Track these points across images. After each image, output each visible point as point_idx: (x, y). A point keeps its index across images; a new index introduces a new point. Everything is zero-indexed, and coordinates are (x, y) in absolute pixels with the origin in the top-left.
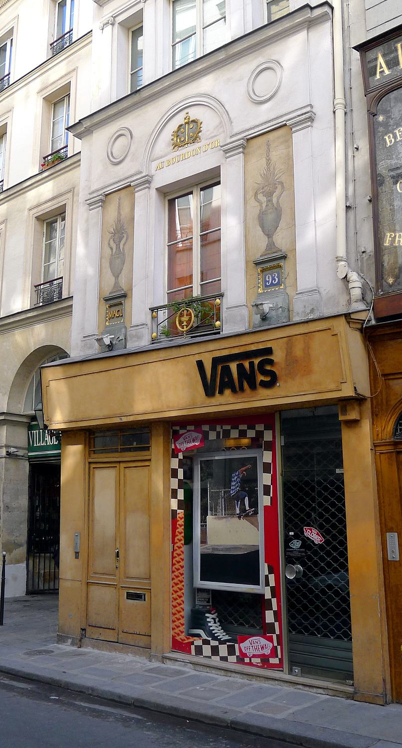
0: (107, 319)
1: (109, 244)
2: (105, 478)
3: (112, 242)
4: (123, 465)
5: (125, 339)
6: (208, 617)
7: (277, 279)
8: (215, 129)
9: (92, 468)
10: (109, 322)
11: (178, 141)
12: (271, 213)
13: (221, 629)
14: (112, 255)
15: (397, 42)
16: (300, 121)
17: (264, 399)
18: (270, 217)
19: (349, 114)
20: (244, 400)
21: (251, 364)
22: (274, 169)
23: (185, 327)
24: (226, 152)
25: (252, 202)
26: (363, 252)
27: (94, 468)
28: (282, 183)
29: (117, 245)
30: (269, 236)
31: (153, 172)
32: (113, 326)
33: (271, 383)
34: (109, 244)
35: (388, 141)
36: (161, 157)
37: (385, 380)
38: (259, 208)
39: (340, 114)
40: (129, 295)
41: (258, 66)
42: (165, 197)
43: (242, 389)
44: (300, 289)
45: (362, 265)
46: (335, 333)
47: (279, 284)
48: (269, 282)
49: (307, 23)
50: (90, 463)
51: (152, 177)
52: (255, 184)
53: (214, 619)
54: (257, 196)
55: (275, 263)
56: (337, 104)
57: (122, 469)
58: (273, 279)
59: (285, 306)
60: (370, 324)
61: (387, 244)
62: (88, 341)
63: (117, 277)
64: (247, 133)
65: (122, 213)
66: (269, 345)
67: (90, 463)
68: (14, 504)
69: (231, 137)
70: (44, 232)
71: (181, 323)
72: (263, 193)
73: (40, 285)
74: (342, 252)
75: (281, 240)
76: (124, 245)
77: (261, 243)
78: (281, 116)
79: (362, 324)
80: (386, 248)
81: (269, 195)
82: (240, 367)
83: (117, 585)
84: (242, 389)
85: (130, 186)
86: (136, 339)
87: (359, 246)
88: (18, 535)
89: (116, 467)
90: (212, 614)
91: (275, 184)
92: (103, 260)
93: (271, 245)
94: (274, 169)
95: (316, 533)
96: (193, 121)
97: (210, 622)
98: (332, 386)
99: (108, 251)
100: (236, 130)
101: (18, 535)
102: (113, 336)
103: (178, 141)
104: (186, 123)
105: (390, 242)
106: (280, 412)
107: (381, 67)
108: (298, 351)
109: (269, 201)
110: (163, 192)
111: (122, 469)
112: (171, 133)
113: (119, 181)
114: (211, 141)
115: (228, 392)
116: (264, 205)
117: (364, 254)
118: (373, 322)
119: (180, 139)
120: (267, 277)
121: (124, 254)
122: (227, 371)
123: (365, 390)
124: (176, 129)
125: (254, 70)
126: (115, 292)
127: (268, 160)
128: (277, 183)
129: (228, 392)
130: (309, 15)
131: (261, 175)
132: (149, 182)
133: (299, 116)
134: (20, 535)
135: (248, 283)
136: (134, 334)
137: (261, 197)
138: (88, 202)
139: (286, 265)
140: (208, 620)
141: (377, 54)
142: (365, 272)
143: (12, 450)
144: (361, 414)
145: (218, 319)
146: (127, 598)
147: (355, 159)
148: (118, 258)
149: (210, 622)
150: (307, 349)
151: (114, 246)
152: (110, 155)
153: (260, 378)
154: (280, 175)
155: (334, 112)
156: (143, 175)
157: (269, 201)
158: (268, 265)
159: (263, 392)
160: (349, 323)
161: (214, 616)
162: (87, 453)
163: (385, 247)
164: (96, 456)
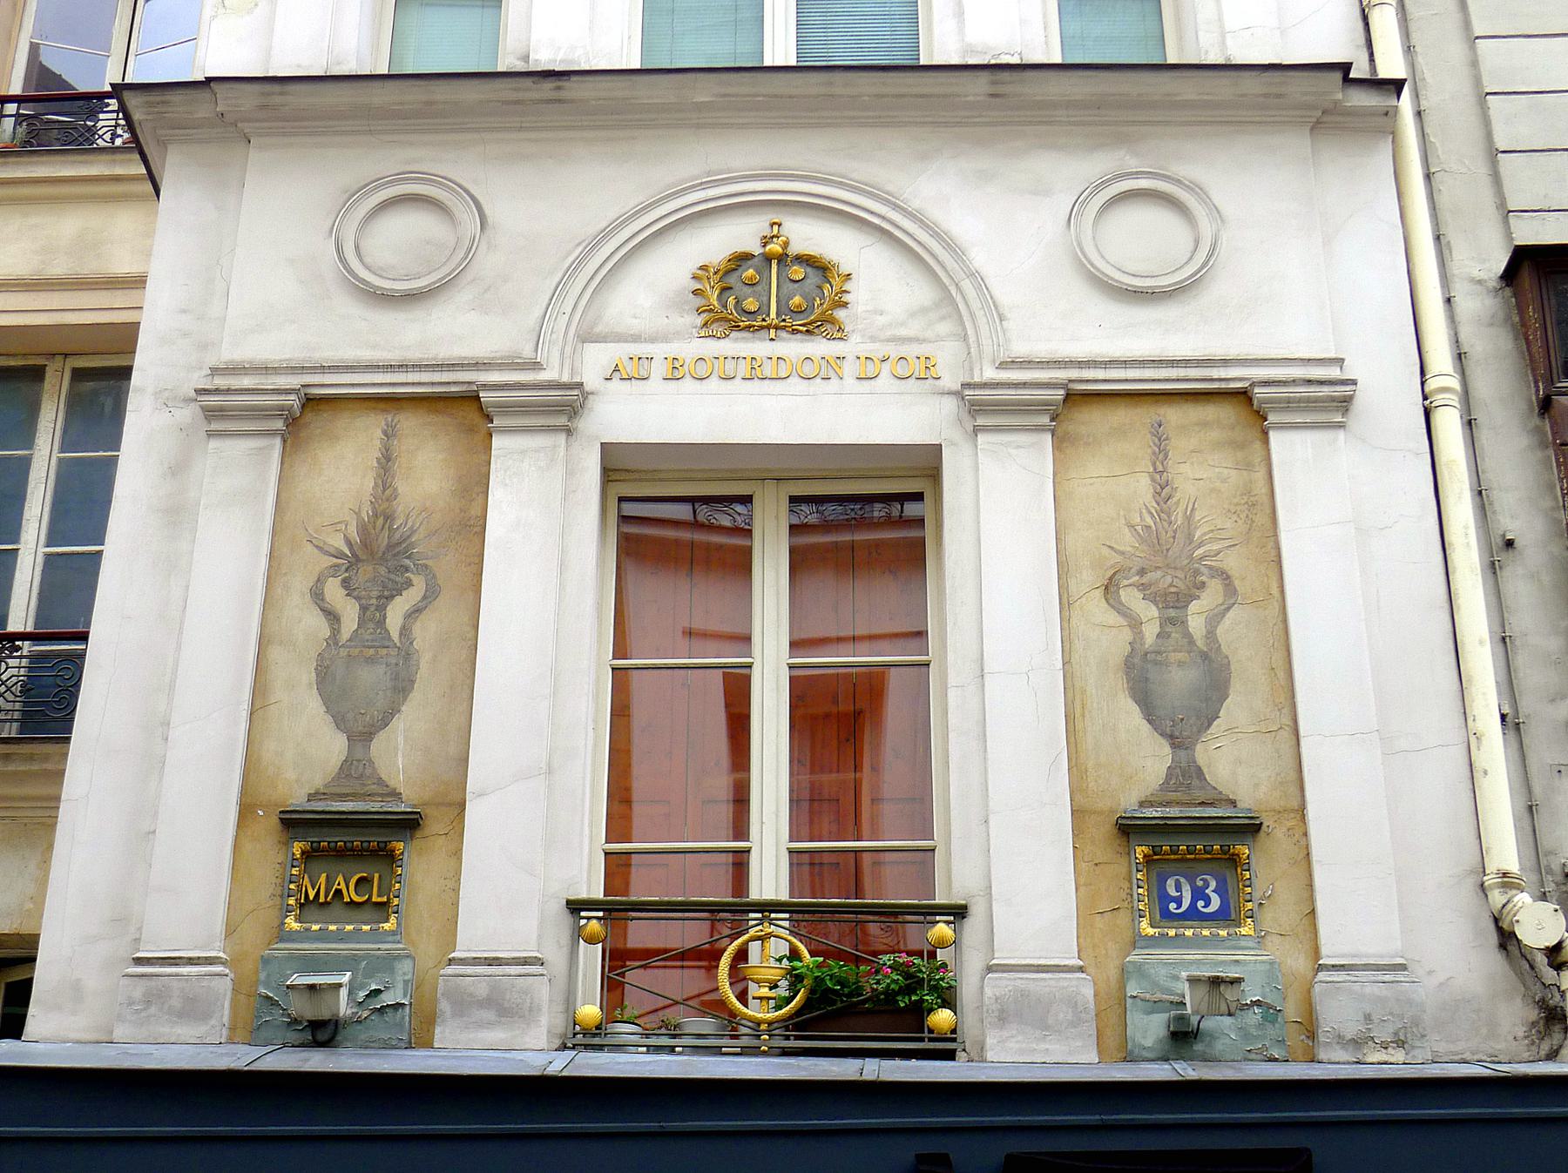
0: (292, 901)
1: (317, 595)
3: (334, 591)
8: (913, 315)
10: (299, 919)
12: (1180, 664)
18: (1179, 680)
25: (1095, 608)
28: (1226, 577)
29: (364, 609)
31: (591, 378)
32: (341, 940)
36: (636, 338)
38: (1127, 635)
39: (1449, 423)
40: (434, 825)
44: (1333, 947)
48: (1179, 902)
51: (586, 395)
52: (1106, 551)
55: (374, 839)
58: (1198, 894)
62: (175, 984)
63: (361, 735)
64: (1074, 374)
65: (402, 486)
69: (1003, 365)
72: (1142, 587)
74: (1506, 854)
78: (1225, 362)
81: (1174, 603)
85: (471, 398)
86: (489, 1015)
87: (1549, 853)
91: (1197, 572)
92: (276, 654)
93: (1186, 774)
94: (1189, 518)
96: (806, 260)
99: (308, 625)
104: (768, 259)
112: (692, 266)
113: (402, 367)
114: (893, 351)
116: (1150, 632)
120: (1170, 883)
125: (1105, 184)
126: (343, 797)
127: (1163, 490)
131: (1132, 527)
135: (1082, 889)
137: (1131, 598)
145: (948, 999)
148: (371, 661)
155: (1427, 414)
156: (543, 376)
157: (1173, 619)
158: (339, 839)
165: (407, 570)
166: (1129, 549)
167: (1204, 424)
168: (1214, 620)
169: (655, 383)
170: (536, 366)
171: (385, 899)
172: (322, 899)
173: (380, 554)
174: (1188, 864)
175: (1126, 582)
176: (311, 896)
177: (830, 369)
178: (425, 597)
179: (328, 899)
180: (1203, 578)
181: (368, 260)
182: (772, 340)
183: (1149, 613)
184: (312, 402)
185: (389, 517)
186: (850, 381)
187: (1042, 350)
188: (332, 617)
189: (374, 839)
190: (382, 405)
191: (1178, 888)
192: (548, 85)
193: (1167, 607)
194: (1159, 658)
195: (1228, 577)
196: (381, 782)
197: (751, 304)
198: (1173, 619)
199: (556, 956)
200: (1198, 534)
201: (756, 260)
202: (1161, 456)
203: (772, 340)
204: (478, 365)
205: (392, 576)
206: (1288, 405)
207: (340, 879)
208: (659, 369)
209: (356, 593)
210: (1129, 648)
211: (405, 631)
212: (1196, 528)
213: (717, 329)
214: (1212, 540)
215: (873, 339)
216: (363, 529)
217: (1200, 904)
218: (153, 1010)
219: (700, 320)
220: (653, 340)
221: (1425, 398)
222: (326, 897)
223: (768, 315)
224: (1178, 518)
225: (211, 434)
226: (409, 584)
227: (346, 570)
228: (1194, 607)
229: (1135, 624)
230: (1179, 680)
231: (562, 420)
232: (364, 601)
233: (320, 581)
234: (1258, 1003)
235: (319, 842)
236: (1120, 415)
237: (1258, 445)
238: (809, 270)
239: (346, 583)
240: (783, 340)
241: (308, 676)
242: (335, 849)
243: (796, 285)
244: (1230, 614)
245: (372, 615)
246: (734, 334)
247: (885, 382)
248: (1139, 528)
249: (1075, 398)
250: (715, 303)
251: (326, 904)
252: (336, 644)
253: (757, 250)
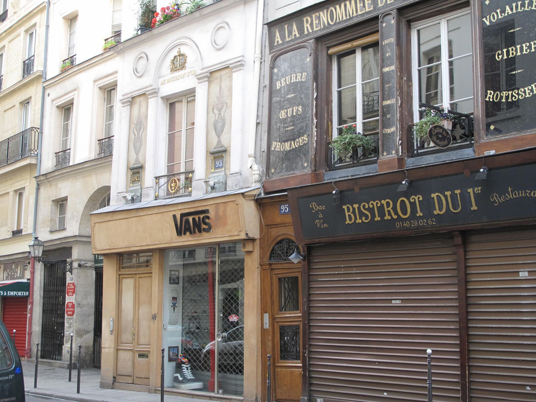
1: (133, 132)
2: (128, 284)
3: (135, 130)
4: (138, 276)
5: (141, 195)
6: (183, 367)
7: (221, 164)
9: (121, 278)
10: (133, 184)
11: (174, 67)
13: (190, 372)
14: (135, 139)
15: (285, 24)
17: (206, 238)
18: (220, 125)
19: (263, 63)
20: (196, 239)
21: (199, 218)
22: (223, 94)
23: (173, 190)
25: (211, 114)
26: (263, 152)
27: (122, 278)
28: (226, 103)
33: (208, 230)
34: (133, 132)
37: (267, 228)
41: (217, 25)
42: (167, 101)
43: (195, 232)
45: (262, 160)
46: (237, 203)
47: (222, 167)
50: (120, 275)
52: (213, 102)
53: (187, 368)
56: (256, 57)
57: (137, 278)
58: (220, 164)
59: (224, 182)
60: (259, 197)
61: (273, 149)
63: (137, 154)
64: (209, 69)
66: (207, 208)
67: (120, 275)
68: (84, 302)
69: (201, 70)
70: (105, 98)
71: (171, 187)
73: (102, 140)
75: (224, 142)
76: (142, 133)
77: (214, 140)
79: (255, 197)
80: (273, 151)
82: (194, 219)
83: (133, 349)
84: (195, 232)
86: (146, 196)
88: (87, 324)
89: (134, 277)
90: (186, 365)
94: (223, 94)
95: (234, 316)
97: (184, 369)
98: (236, 233)
99: (133, 136)
100: (206, 65)
101: (87, 324)
102: (134, 194)
103: (174, 67)
106: (219, 244)
107: (277, 38)
108: (221, 213)
109: (220, 114)
111: (137, 278)
115: (188, 233)
118: (263, 195)
122: (187, 221)
123: (255, 233)
124: (172, 58)
125: (215, 27)
129: (188, 233)
132: (156, 93)
134: (89, 324)
136: (145, 193)
137: (215, 110)
140: (183, 368)
141: (276, 31)
142: (264, 164)
143: (82, 262)
144: (253, 247)
146: (139, 357)
147: (264, 93)
149: (184, 369)
150: (225, 211)
151: (136, 133)
152: (136, 70)
153: (204, 226)
155: (254, 62)
156: (153, 87)
157: (220, 114)
159: (205, 234)
160: (244, 197)
161: (187, 366)
162: (118, 268)
163: (272, 150)
164: (123, 270)
167: (226, 74)
170: (152, 86)
181: (217, 42)
184: (211, 73)
190: (139, 97)
196: (139, 161)
199: (155, 186)
204: (147, 87)
206: (235, 67)
207: (508, 8)
225: (199, 83)
230: (220, 125)
234: (221, 182)
246: (175, 72)
253: (177, 54)
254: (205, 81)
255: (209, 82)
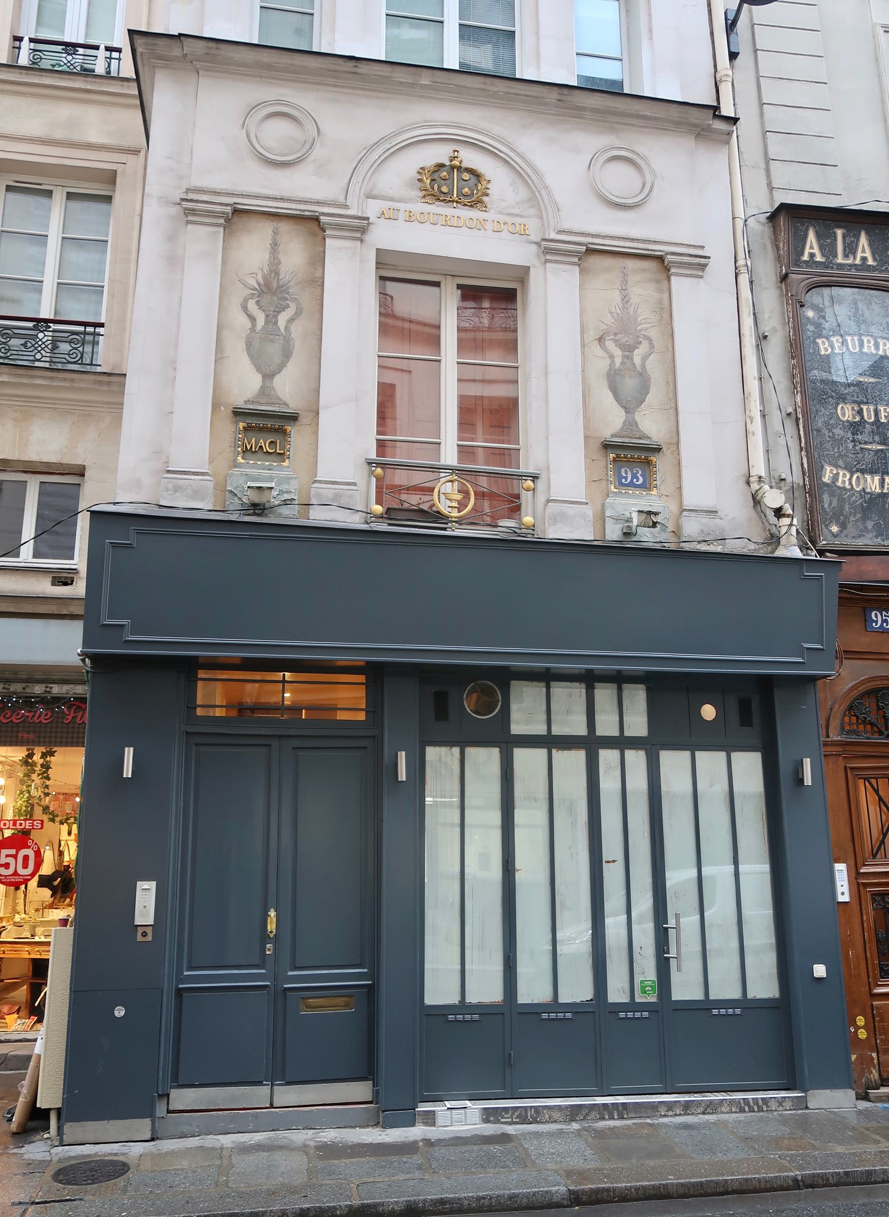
0: (240, 449)
3: (252, 306)
11: (436, 187)
16: (690, 264)
18: (629, 384)
24: (547, 251)
28: (649, 339)
29: (267, 316)
30: (268, 376)
31: (371, 214)
35: (822, 347)
36: (392, 199)
48: (626, 478)
49: (699, 130)
52: (600, 323)
54: (604, 342)
55: (277, 424)
58: (634, 476)
69: (560, 232)
72: (615, 341)
81: (628, 349)
91: (638, 337)
93: (631, 424)
94: (635, 312)
105: (831, 478)
110: (384, 259)
112: (417, 167)
113: (282, 199)
116: (618, 361)
117: (783, 483)
119: (439, 188)
120: (623, 470)
121: (288, 340)
128: (641, 336)
130: (711, 122)
133: (691, 256)
137: (610, 344)
138: (189, 205)
139: (297, 436)
154: (646, 326)
157: (627, 358)
158: (261, 422)
165: (287, 299)
166: (610, 323)
167: (644, 270)
168: (644, 359)
169: (401, 222)
171: (282, 452)
172: (253, 450)
173: (274, 290)
174: (630, 462)
175: (609, 338)
176: (249, 447)
177: (480, 226)
178: (296, 313)
179: (257, 450)
180: (641, 339)
182: (455, 208)
183: (618, 353)
185: (277, 273)
186: (490, 232)
187: (576, 227)
188: (253, 319)
189: (277, 424)
190: (271, 218)
191: (626, 473)
192: (351, 64)
193: (625, 351)
194: (621, 373)
195: (651, 340)
197: (445, 189)
198: (627, 358)
200: (639, 319)
201: (447, 168)
202: (625, 282)
203: (455, 208)
204: (318, 203)
205: (280, 302)
206: (681, 265)
207: (262, 441)
208: (402, 215)
209: (262, 308)
210: (609, 368)
211: (287, 328)
212: (639, 317)
213: (428, 199)
214: (644, 323)
215: (500, 213)
216: (265, 277)
217: (635, 480)
218: (178, 494)
219: (421, 194)
220: (399, 201)
221: (736, 269)
222: (255, 449)
223: (453, 195)
224: (631, 310)
226: (288, 306)
227: (258, 297)
228: (636, 352)
229: (612, 357)
230: (629, 384)
231: (358, 235)
232: (267, 313)
233: (246, 300)
235: (251, 424)
236: (607, 261)
237: (666, 282)
238: (471, 175)
239: (258, 303)
240: (460, 208)
241: (242, 345)
242: (258, 427)
243: (465, 183)
244: (652, 356)
245: (271, 320)
246: (437, 203)
247: (505, 234)
248: (614, 314)
249: (591, 251)
250: (429, 187)
251: (255, 452)
252: (255, 331)
254: (574, 264)
255: (582, 271)
